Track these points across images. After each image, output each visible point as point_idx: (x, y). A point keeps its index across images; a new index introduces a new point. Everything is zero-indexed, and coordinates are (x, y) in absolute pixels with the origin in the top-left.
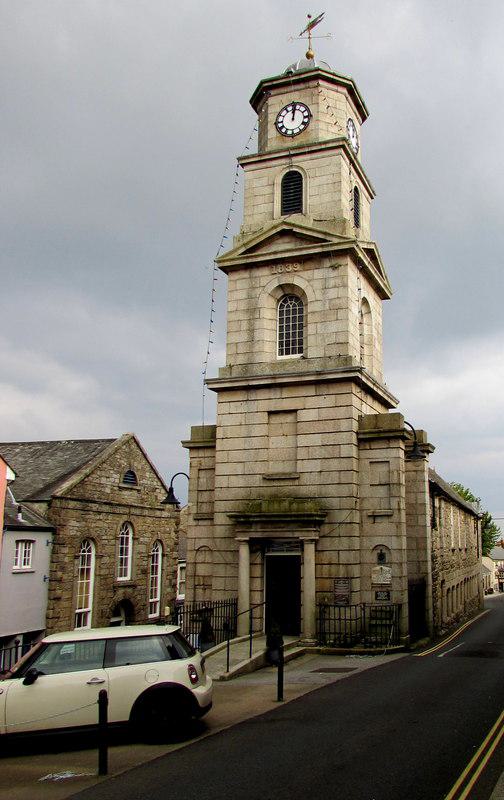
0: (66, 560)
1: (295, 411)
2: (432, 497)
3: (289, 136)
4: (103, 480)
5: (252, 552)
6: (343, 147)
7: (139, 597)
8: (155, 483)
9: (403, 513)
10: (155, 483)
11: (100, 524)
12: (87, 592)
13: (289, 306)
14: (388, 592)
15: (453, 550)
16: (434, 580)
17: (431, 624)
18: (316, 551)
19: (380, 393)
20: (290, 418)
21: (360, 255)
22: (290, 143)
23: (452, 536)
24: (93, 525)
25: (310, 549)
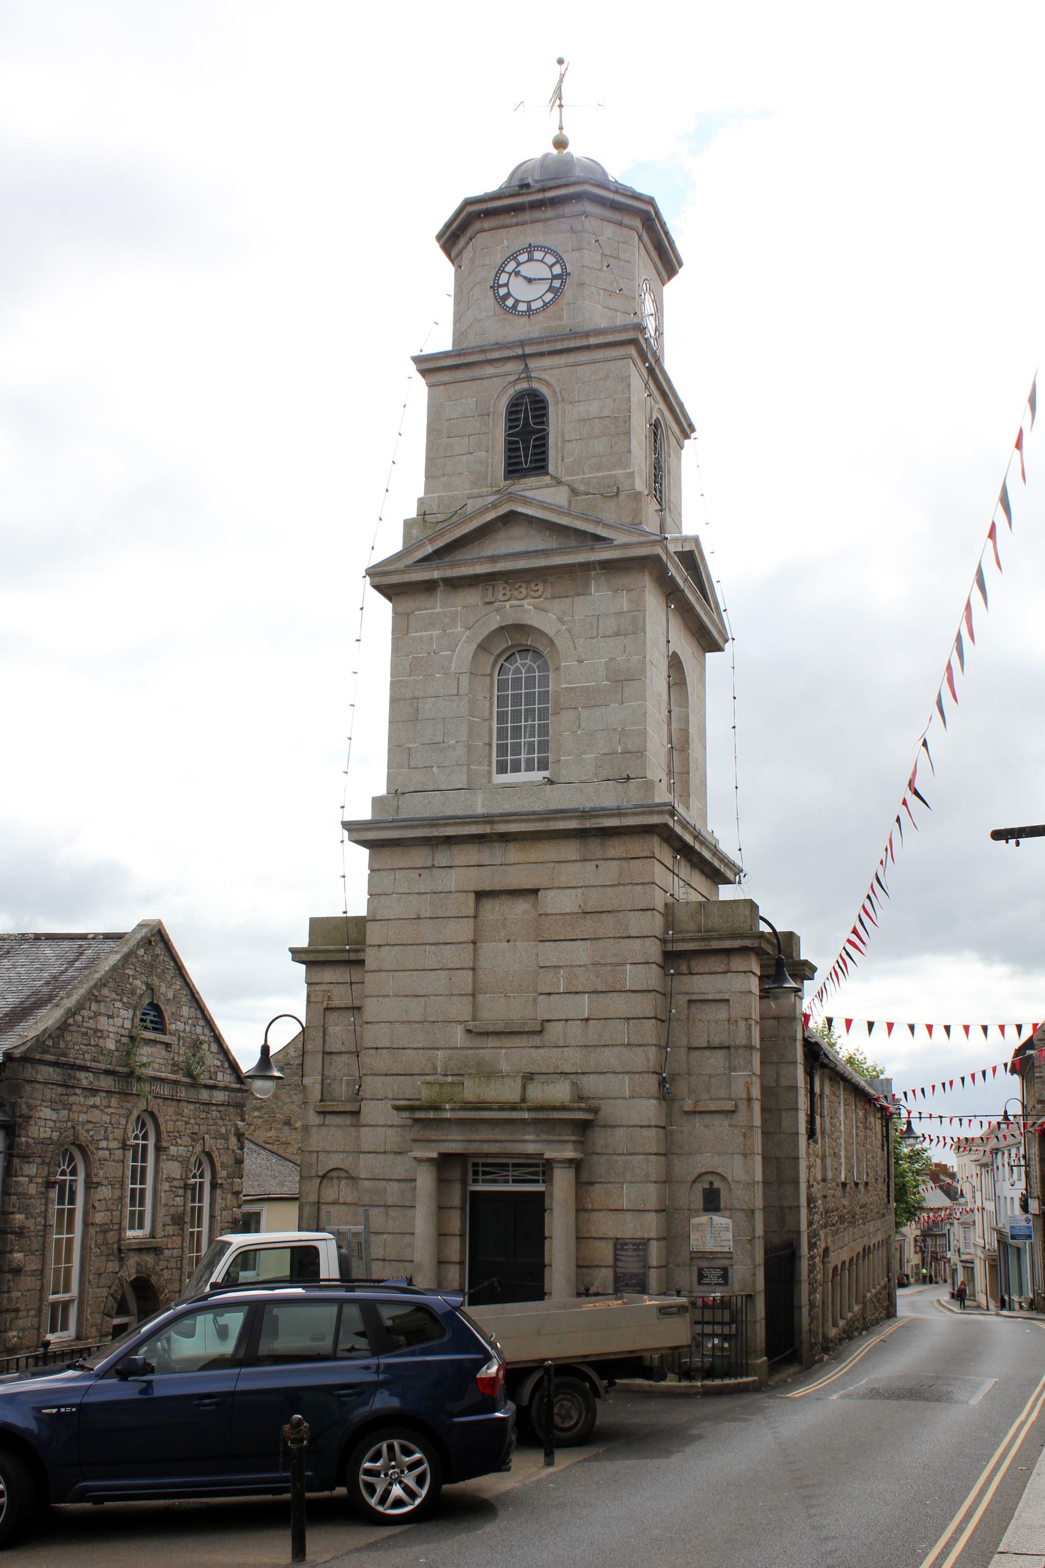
0: (32, 1190)
1: (535, 891)
2: (810, 1074)
3: (522, 314)
4: (103, 1023)
5: (442, 1181)
6: (634, 342)
7: (166, 1274)
8: (199, 1030)
9: (757, 1106)
10: (199, 1030)
11: (95, 1115)
12: (69, 1259)
13: (517, 671)
14: (725, 1270)
15: (844, 1185)
16: (812, 1246)
17: (805, 1336)
18: (577, 1183)
19: (707, 855)
20: (521, 907)
21: (673, 571)
22: (519, 329)
23: (842, 1154)
24: (83, 1118)
25: (562, 1183)
